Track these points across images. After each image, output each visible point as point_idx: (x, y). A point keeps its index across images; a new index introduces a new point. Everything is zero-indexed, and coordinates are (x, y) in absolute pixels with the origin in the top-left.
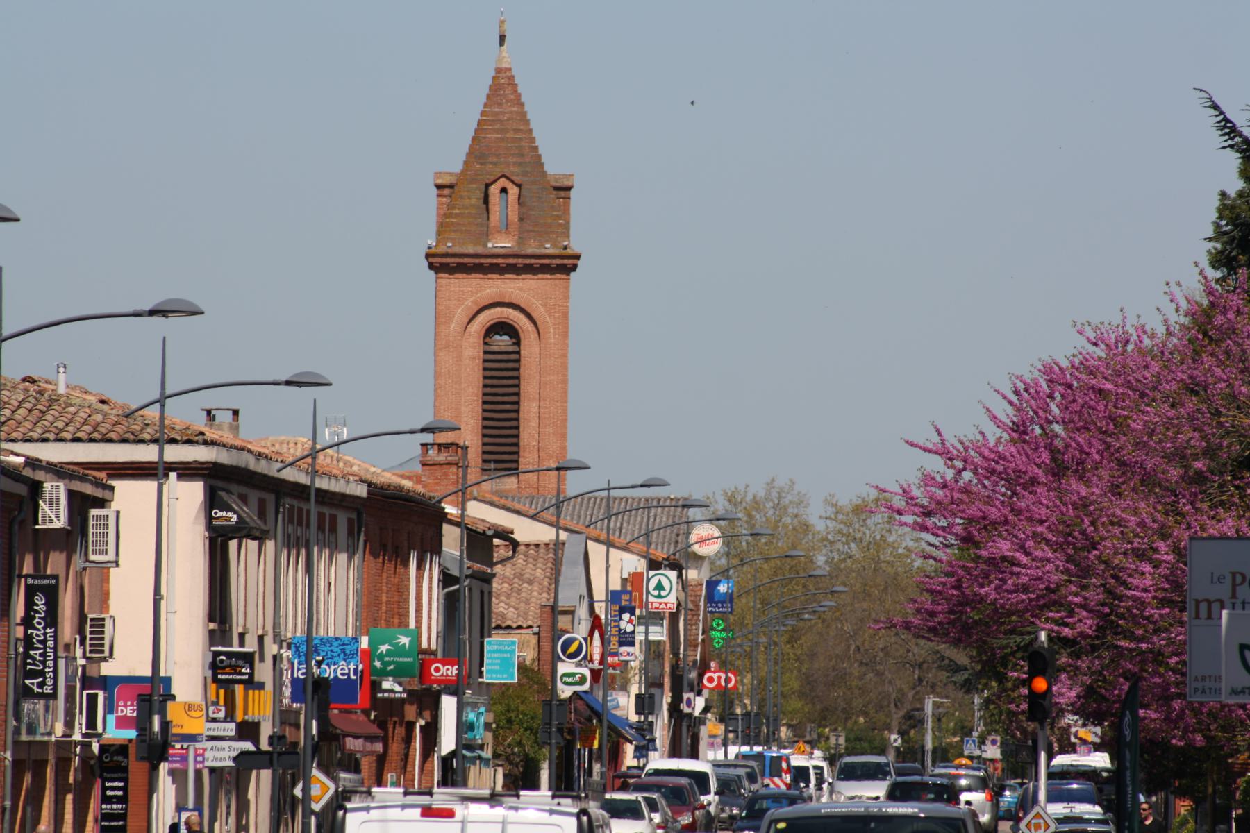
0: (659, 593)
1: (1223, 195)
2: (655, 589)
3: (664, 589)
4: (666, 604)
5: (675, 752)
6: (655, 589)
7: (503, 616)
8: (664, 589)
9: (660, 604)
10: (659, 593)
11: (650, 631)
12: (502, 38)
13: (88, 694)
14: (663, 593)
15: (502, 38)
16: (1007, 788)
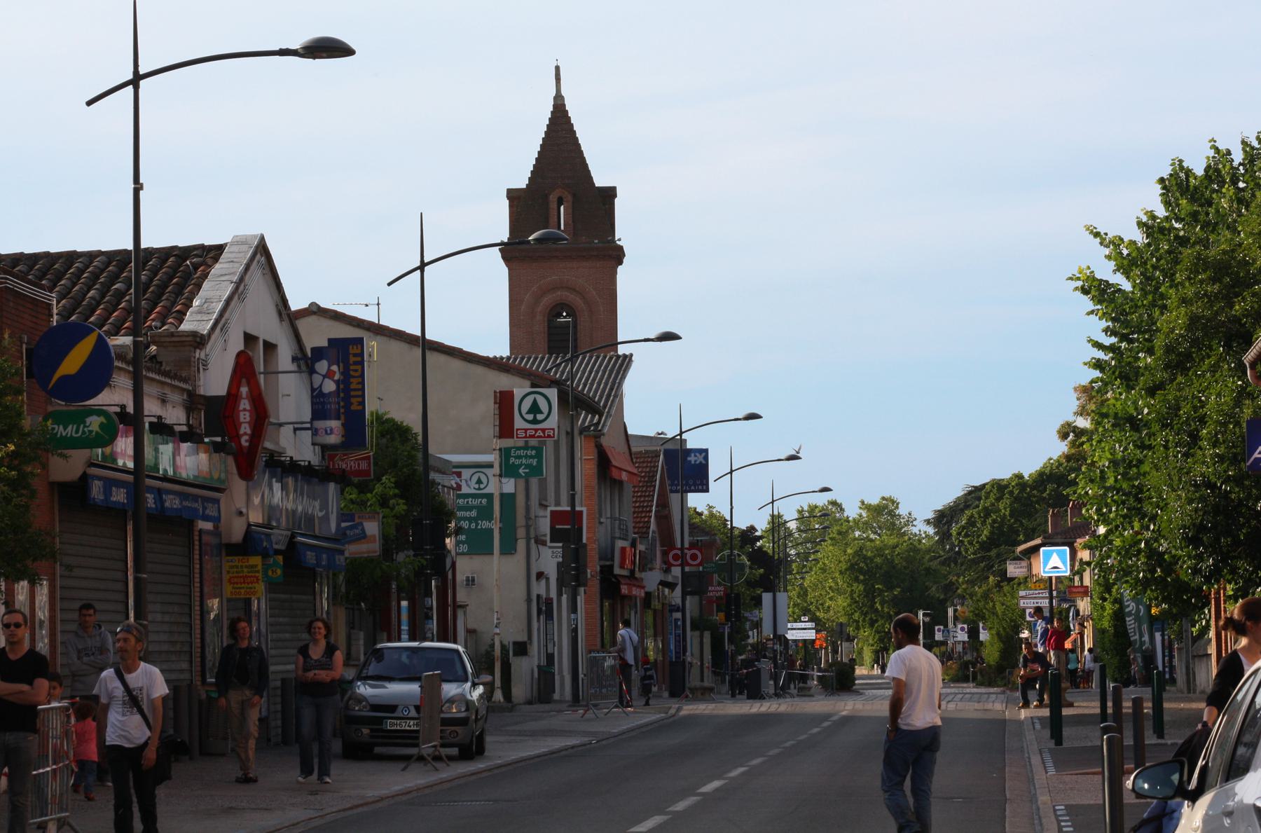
0: (535, 417)
1: (1080, 267)
2: (529, 412)
3: (541, 412)
4: (543, 430)
5: (412, 639)
6: (529, 412)
7: (149, 411)
8: (541, 412)
9: (536, 430)
10: (535, 417)
11: (1047, 601)
12: (753, 416)
13: (551, 541)
14: (540, 417)
15: (753, 416)
16: (684, 448)
